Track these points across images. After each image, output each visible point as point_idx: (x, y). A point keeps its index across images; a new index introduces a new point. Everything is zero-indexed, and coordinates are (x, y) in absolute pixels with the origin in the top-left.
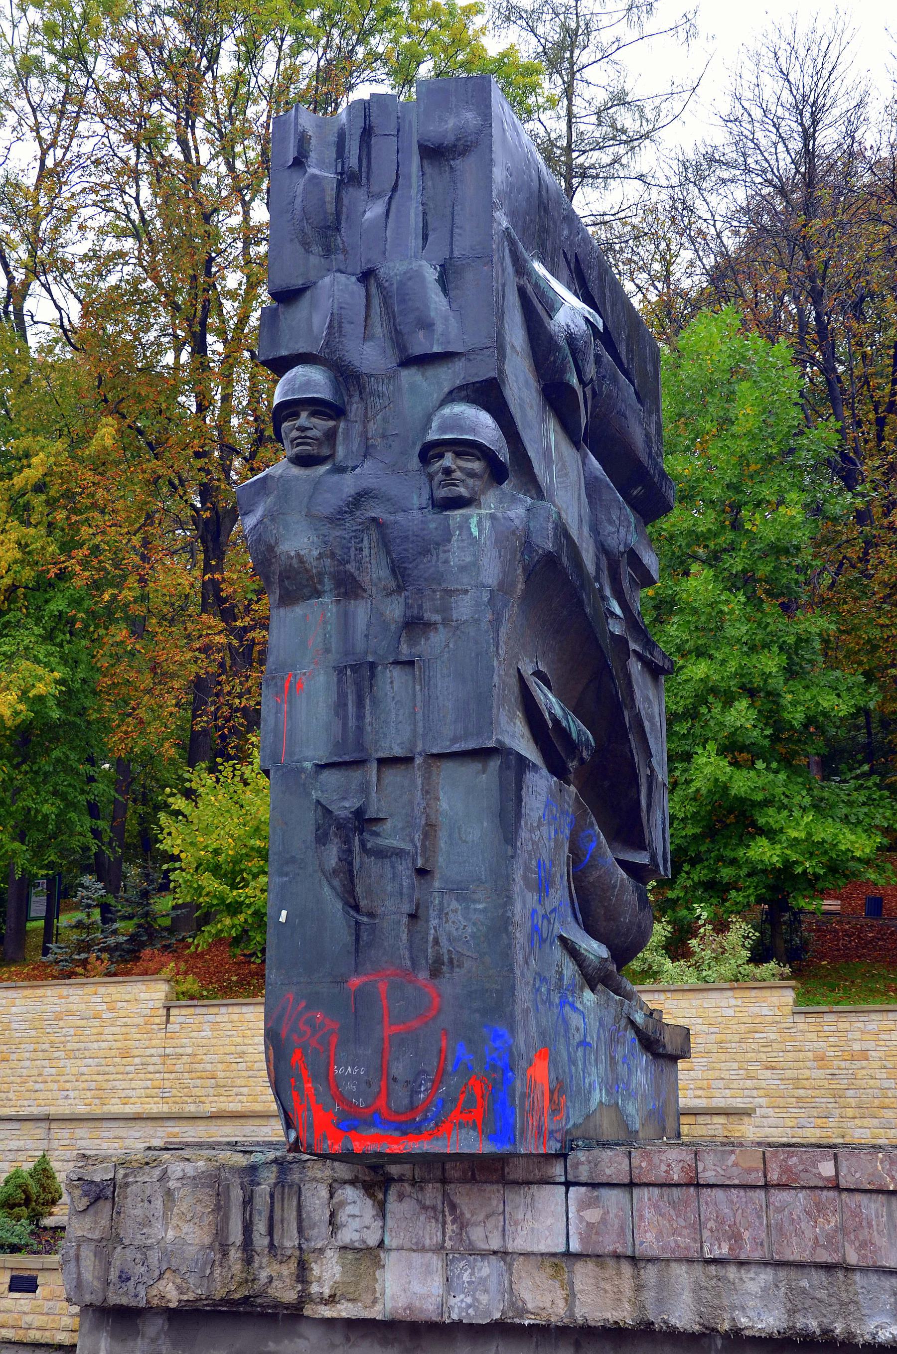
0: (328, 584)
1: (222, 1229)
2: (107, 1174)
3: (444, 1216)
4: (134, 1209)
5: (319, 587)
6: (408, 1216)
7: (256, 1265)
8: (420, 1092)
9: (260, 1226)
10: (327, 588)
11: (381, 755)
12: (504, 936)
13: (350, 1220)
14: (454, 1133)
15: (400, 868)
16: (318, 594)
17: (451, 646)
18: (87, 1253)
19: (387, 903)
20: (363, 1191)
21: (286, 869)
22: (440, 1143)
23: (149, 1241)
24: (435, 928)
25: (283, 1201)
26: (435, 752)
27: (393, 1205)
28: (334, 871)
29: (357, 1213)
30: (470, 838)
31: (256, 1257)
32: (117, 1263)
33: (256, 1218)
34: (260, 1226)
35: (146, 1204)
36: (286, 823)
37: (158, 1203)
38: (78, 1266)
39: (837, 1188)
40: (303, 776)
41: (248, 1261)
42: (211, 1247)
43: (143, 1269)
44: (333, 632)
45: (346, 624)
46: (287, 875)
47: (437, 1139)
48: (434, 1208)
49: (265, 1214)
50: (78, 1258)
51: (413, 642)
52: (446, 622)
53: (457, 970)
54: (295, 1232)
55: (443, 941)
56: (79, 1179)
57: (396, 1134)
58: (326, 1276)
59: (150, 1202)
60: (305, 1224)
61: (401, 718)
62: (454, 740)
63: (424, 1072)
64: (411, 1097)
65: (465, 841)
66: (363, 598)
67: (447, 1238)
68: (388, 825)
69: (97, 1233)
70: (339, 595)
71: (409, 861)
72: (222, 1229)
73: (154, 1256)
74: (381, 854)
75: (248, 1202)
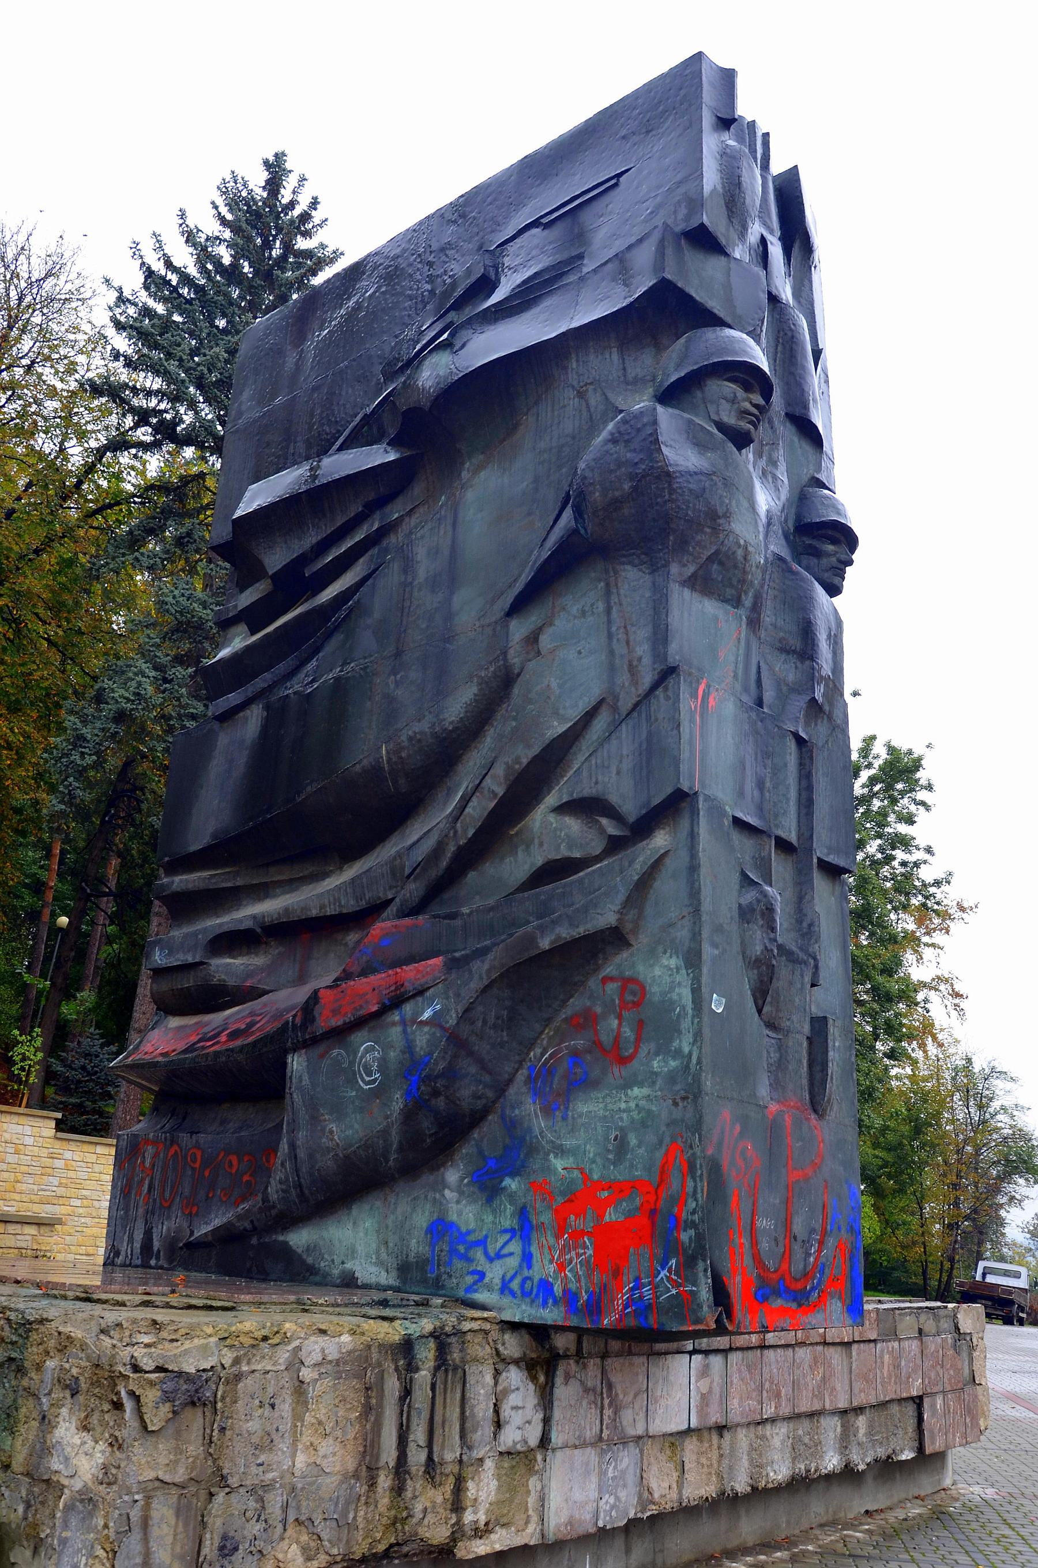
1: (372, 1441)
2: (205, 1358)
3: (602, 1399)
4: (249, 1421)
6: (573, 1402)
7: (409, 1494)
9: (418, 1434)
13: (513, 1413)
18: (163, 1511)
20: (526, 1374)
23: (270, 1475)
25: (445, 1394)
27: (564, 1392)
29: (520, 1404)
31: (409, 1482)
32: (216, 1524)
33: (415, 1420)
34: (418, 1434)
35: (267, 1411)
37: (285, 1407)
38: (146, 1539)
39: (825, 1343)
41: (398, 1490)
42: (356, 1476)
43: (256, 1528)
48: (594, 1390)
49: (425, 1415)
50: (145, 1523)
54: (457, 1438)
56: (160, 1369)
58: (483, 1496)
59: (273, 1406)
60: (468, 1425)
67: (604, 1427)
69: (181, 1470)
72: (372, 1446)
73: (275, 1501)
75: (407, 1392)
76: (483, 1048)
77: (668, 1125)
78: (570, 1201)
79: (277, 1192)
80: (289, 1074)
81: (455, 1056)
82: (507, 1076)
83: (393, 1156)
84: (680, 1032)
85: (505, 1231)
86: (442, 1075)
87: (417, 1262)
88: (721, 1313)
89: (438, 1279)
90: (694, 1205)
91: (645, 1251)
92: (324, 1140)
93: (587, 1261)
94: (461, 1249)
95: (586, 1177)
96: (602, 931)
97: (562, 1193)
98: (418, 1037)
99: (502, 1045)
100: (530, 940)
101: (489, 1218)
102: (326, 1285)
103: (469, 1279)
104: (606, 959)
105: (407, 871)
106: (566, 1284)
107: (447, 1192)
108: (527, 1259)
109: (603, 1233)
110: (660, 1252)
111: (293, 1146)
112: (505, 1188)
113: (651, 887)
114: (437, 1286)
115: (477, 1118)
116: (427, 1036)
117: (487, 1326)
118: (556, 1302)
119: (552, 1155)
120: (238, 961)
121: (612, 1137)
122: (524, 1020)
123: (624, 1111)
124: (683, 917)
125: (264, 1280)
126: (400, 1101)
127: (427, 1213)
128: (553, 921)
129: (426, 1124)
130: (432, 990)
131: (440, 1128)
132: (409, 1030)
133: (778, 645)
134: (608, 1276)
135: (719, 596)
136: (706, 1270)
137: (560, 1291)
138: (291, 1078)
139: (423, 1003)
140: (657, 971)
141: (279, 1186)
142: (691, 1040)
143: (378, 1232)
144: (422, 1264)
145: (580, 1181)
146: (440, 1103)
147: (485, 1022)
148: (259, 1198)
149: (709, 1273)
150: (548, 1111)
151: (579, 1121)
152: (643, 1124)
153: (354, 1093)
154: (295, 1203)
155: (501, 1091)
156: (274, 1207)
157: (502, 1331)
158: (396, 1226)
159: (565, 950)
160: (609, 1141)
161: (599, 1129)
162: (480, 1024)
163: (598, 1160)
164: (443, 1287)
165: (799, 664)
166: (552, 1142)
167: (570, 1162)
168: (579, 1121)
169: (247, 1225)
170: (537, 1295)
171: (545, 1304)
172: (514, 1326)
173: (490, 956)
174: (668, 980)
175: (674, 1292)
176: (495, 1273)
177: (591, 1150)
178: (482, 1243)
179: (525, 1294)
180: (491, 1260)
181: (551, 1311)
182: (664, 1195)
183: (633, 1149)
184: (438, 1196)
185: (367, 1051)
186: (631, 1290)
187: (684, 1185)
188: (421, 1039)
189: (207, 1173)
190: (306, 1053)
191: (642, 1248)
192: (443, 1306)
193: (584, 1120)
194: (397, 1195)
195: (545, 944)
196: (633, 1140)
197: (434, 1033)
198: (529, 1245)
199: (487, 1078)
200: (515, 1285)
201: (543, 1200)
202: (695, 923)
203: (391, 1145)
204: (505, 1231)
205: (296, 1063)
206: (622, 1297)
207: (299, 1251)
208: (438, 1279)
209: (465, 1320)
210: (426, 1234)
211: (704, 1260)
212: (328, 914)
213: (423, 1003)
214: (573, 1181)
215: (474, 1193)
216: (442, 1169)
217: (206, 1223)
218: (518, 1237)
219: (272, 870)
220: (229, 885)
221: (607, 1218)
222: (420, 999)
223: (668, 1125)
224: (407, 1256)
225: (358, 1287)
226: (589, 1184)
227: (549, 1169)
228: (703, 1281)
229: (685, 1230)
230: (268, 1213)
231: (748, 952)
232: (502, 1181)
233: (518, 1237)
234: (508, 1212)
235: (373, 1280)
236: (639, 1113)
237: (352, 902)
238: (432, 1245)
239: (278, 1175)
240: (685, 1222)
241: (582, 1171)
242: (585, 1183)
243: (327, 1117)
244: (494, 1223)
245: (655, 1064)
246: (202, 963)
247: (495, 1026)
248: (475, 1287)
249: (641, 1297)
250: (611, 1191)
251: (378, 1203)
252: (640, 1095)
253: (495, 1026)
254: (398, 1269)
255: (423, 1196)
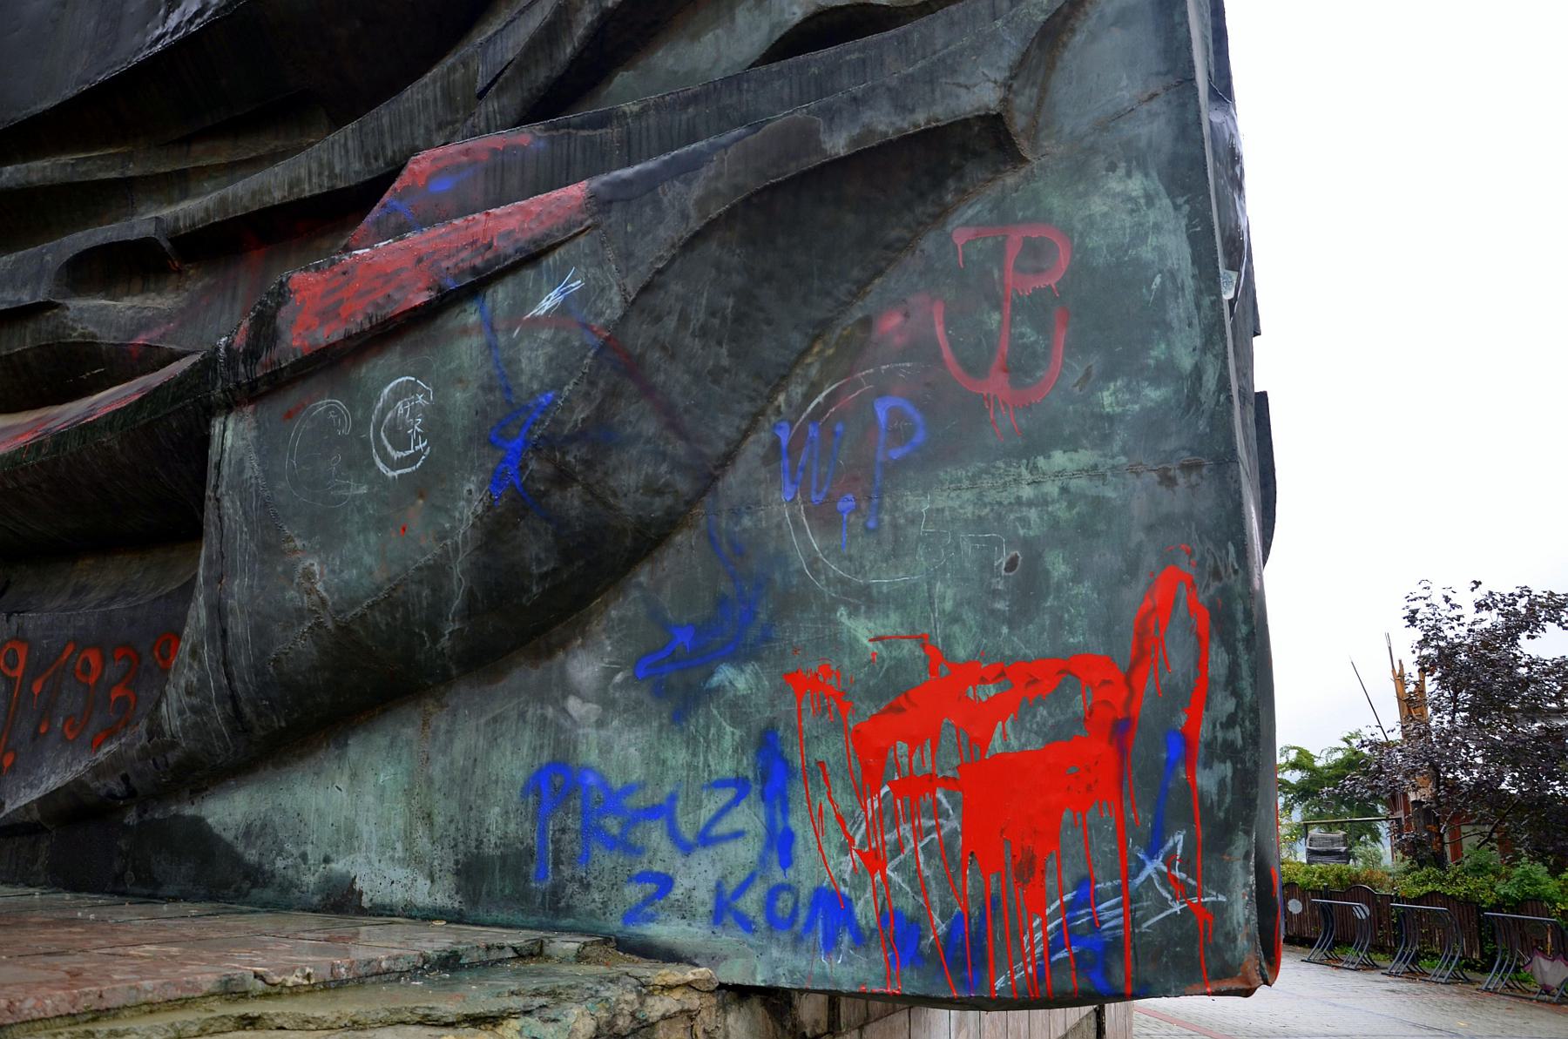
76: (674, 379)
77: (1150, 528)
78: (893, 709)
79: (181, 713)
80: (213, 456)
81: (613, 394)
82: (721, 447)
83: (450, 627)
84: (1166, 327)
85: (722, 784)
86: (578, 436)
87: (503, 857)
89: (556, 892)
90: (1230, 705)
91: (1101, 817)
92: (291, 594)
93: (945, 846)
94: (612, 825)
95: (935, 657)
96: (965, 123)
97: (871, 694)
98: (526, 353)
99: (717, 374)
100: (807, 137)
101: (678, 756)
102: (289, 907)
103: (634, 893)
104: (962, 193)
105: (480, 85)
106: (888, 898)
107: (573, 704)
108: (781, 844)
109: (985, 784)
110: (1142, 817)
111: (218, 611)
112: (719, 689)
113: (1065, 45)
114: (555, 910)
115: (650, 539)
116: (549, 349)
117: (693, 1001)
118: (859, 939)
119: (842, 613)
120: (124, 304)
121: (1004, 561)
122: (769, 322)
123: (1030, 504)
124: (1152, 97)
125: (153, 897)
126: (477, 496)
127: (525, 750)
128: (855, 99)
129: (534, 550)
130: (561, 251)
131: (549, 572)
132: (502, 339)
134: (1002, 880)
136: (1247, 856)
137: (872, 915)
138: (218, 466)
139: (537, 281)
140: (1098, 206)
141: (185, 699)
142: (1198, 342)
143: (408, 793)
144: (516, 861)
145: (921, 665)
146: (572, 500)
147: (684, 319)
148: (143, 725)
149: (1252, 863)
150: (826, 517)
151: (912, 532)
152: (1084, 528)
153: (364, 490)
154: (220, 736)
155: (708, 479)
156: (173, 745)
157: (723, 1008)
158: (452, 780)
159: (873, 160)
160: (994, 572)
161: (967, 547)
162: (671, 323)
163: (969, 616)
164: (569, 910)
166: (841, 581)
167: (891, 623)
168: (912, 532)
169: (115, 785)
170: (809, 925)
171: (830, 944)
172: (740, 993)
173: (707, 172)
174: (1129, 221)
175: (1177, 908)
176: (697, 877)
177: (947, 595)
178: (662, 811)
179: (774, 923)
180: (687, 849)
181: (849, 962)
182: (1150, 686)
183: (1059, 587)
184: (550, 712)
185: (398, 395)
186: (1067, 908)
187: (1202, 663)
188: (533, 360)
189: (37, 687)
190: (254, 412)
191: (1092, 813)
192: (580, 957)
193: (923, 528)
194: (454, 713)
195: (838, 144)
196: (1058, 566)
197: (565, 341)
198: (785, 811)
199: (679, 449)
200: (751, 903)
201: (821, 711)
202: (1183, 106)
203: (449, 601)
204: (722, 784)
205: (232, 435)
206: (1043, 925)
207: (228, 836)
208: (556, 892)
209: (651, 994)
210: (525, 792)
211: (1248, 833)
212: (307, 194)
213: (537, 281)
214: (899, 665)
215: (639, 703)
216: (561, 655)
217: (32, 786)
218: (754, 795)
219: (198, 148)
220: (113, 175)
221: (996, 745)
222: (529, 274)
223: (1150, 528)
224: (480, 843)
225: (362, 911)
226: (944, 671)
227: (839, 643)
228: (1241, 880)
229: (1208, 765)
230: (159, 760)
232: (711, 674)
233: (754, 795)
234: (727, 742)
235: (398, 896)
236: (1071, 506)
237: (357, 166)
238: (540, 817)
239: (184, 674)
240: (1208, 745)
241: (924, 641)
242: (933, 670)
243: (299, 543)
244: (690, 767)
245: (1107, 398)
246: (47, 306)
247: (703, 332)
248: (649, 910)
249: (1095, 924)
250: (1006, 684)
251: (409, 732)
252: (1071, 467)
253: (703, 332)
254: (457, 873)
255: (514, 714)
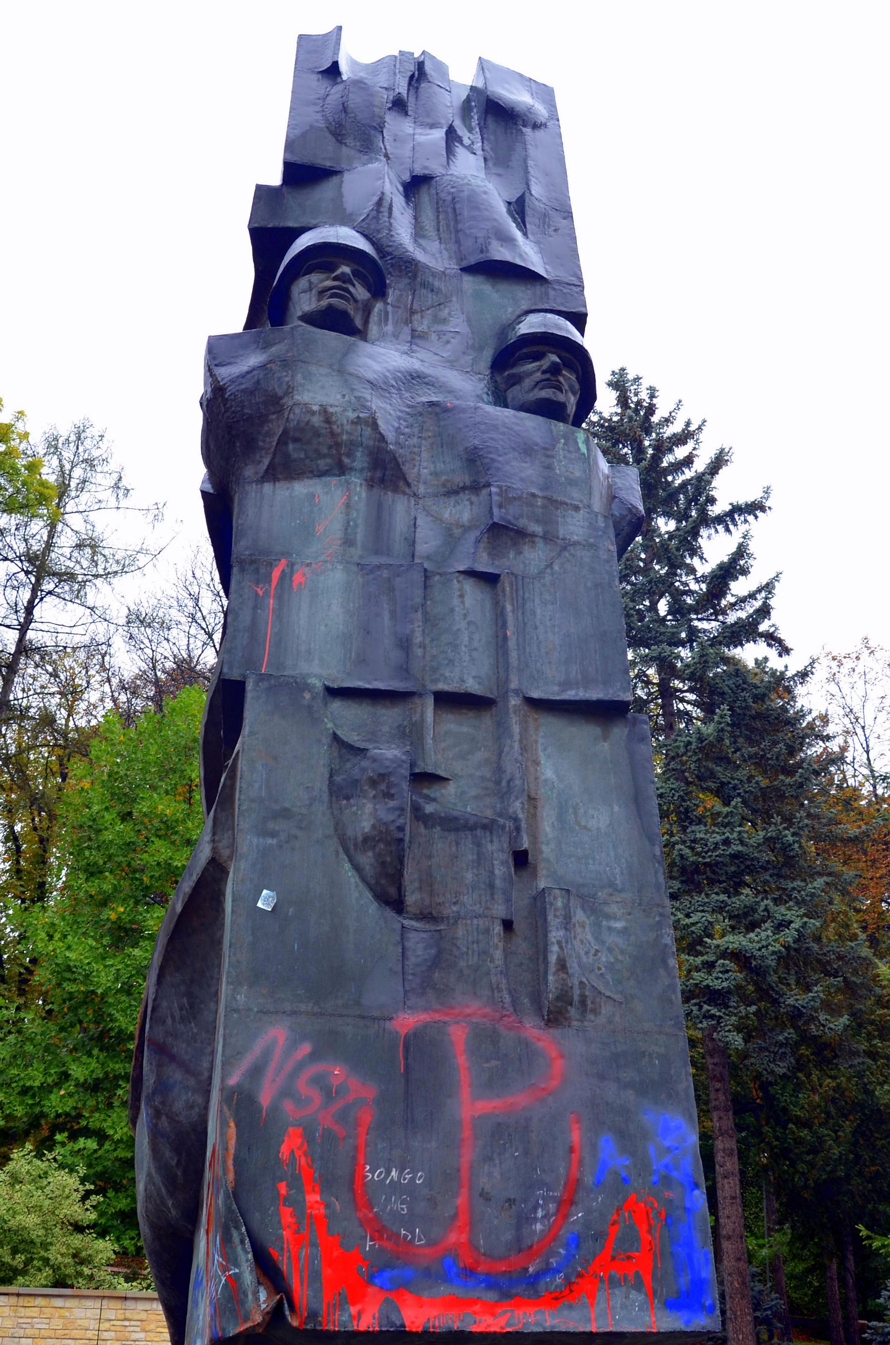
0: (360, 460)
5: (346, 460)
8: (535, 1219)
10: (357, 465)
11: (442, 686)
12: (662, 972)
14: (601, 1296)
15: (489, 847)
16: (341, 469)
17: (556, 567)
19: (465, 899)
21: (271, 825)
22: (575, 1315)
24: (559, 943)
26: (535, 695)
28: (366, 839)
30: (592, 824)
36: (275, 758)
40: (307, 696)
44: (360, 521)
45: (379, 517)
46: (273, 835)
47: (570, 1307)
51: (495, 552)
52: (548, 538)
53: (591, 1017)
55: (573, 966)
57: (491, 1296)
61: (476, 644)
62: (566, 684)
63: (542, 1184)
64: (518, 1227)
65: (585, 828)
66: (404, 493)
68: (451, 789)
70: (372, 479)
71: (505, 839)
74: (452, 824)
88: (281, 1299)
133: (442, 490)
135: (312, 472)
136: (242, 1242)
147: (173, 1017)
162: (169, 1021)
165: (474, 498)
211: (237, 1228)
231: (350, 833)
